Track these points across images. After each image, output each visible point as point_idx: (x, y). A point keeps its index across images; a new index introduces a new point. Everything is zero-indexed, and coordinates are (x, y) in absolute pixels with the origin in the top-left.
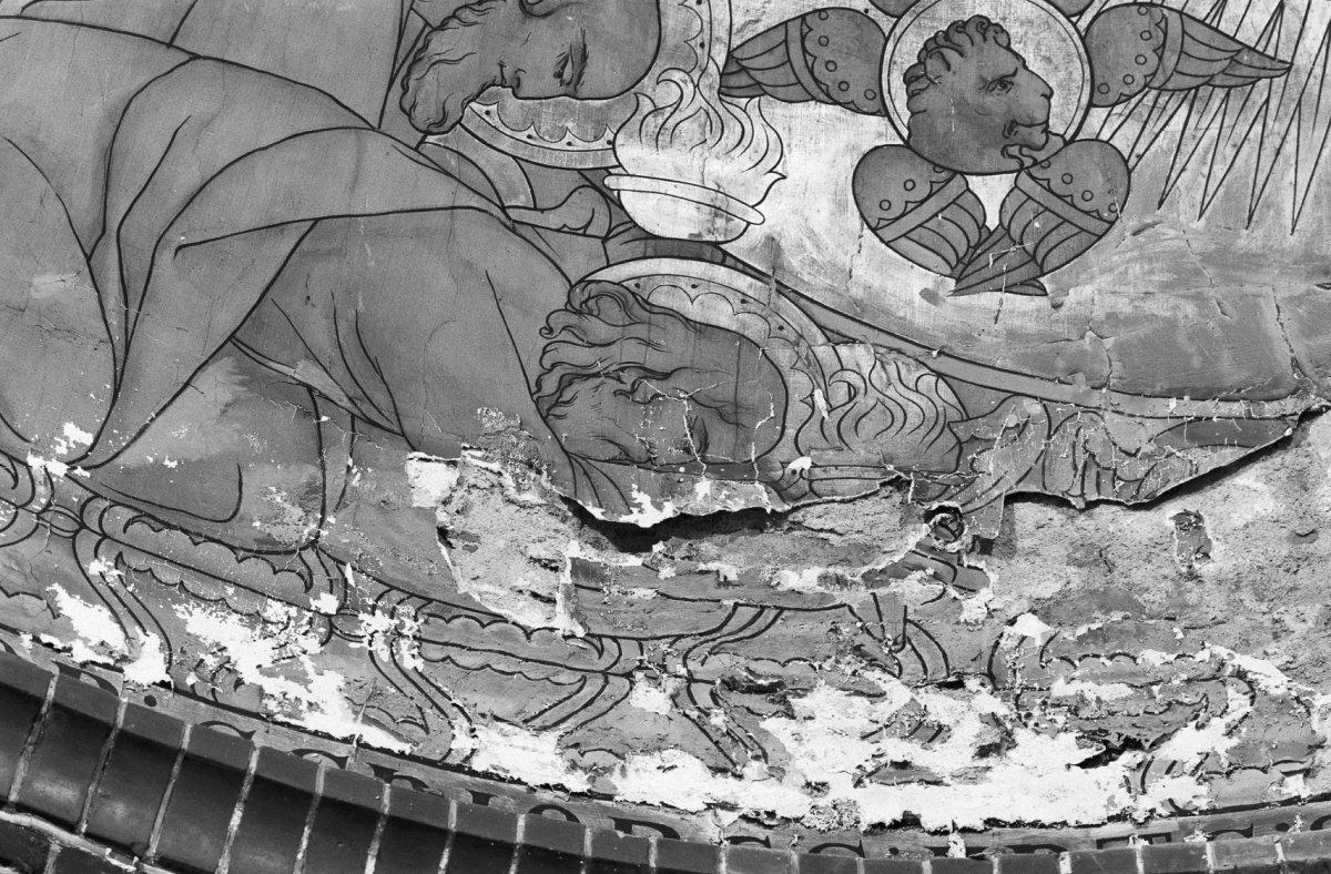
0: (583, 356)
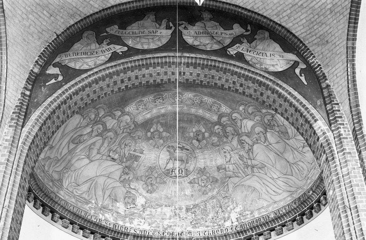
0: (127, 196)
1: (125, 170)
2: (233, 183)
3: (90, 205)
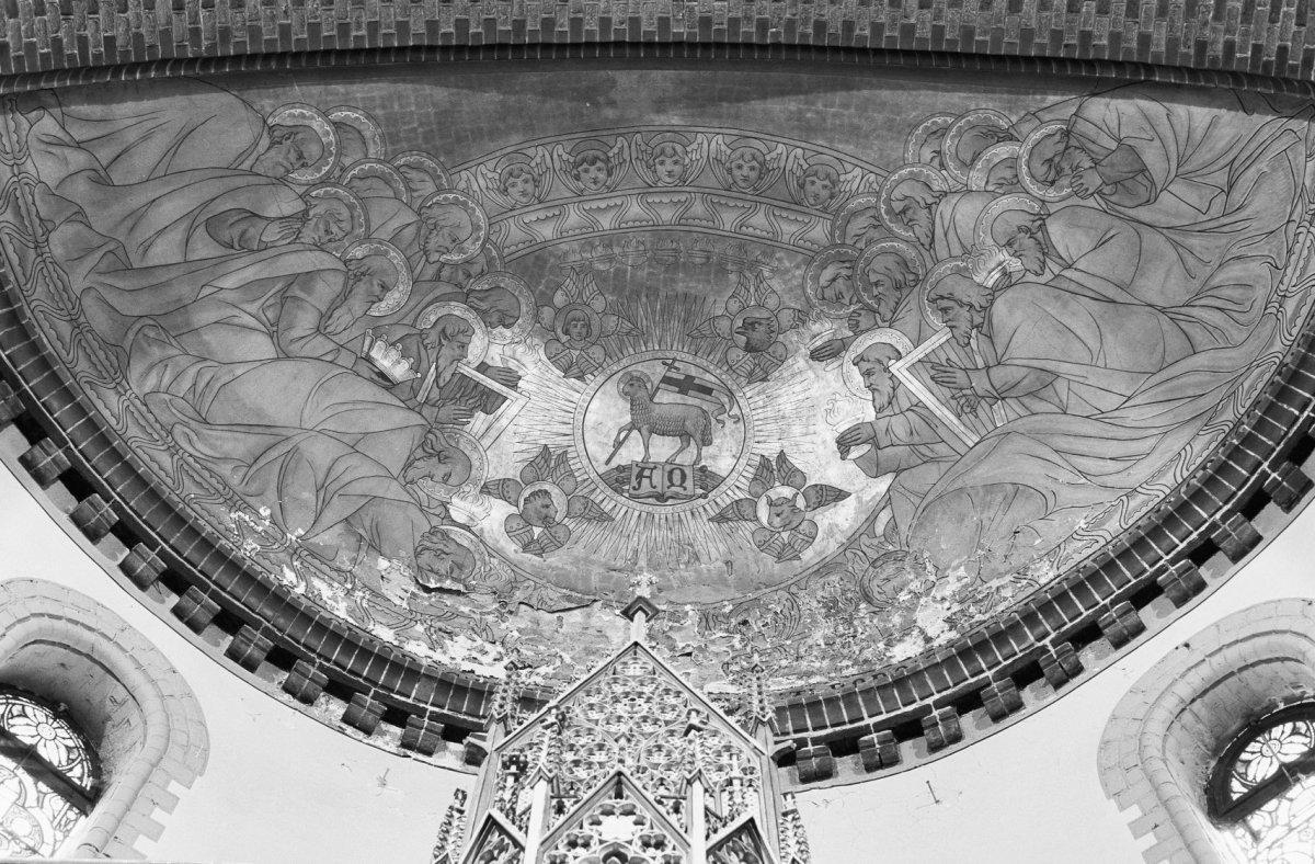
0: (429, 544)
1: (430, 436)
2: (915, 494)
3: (247, 518)
